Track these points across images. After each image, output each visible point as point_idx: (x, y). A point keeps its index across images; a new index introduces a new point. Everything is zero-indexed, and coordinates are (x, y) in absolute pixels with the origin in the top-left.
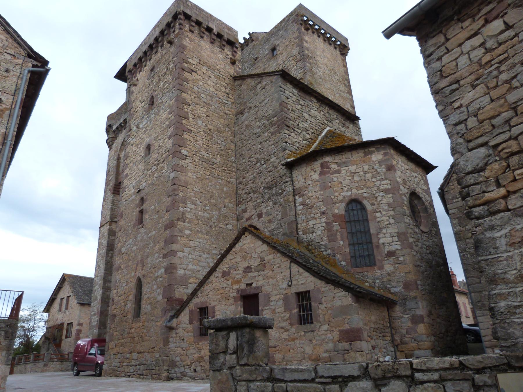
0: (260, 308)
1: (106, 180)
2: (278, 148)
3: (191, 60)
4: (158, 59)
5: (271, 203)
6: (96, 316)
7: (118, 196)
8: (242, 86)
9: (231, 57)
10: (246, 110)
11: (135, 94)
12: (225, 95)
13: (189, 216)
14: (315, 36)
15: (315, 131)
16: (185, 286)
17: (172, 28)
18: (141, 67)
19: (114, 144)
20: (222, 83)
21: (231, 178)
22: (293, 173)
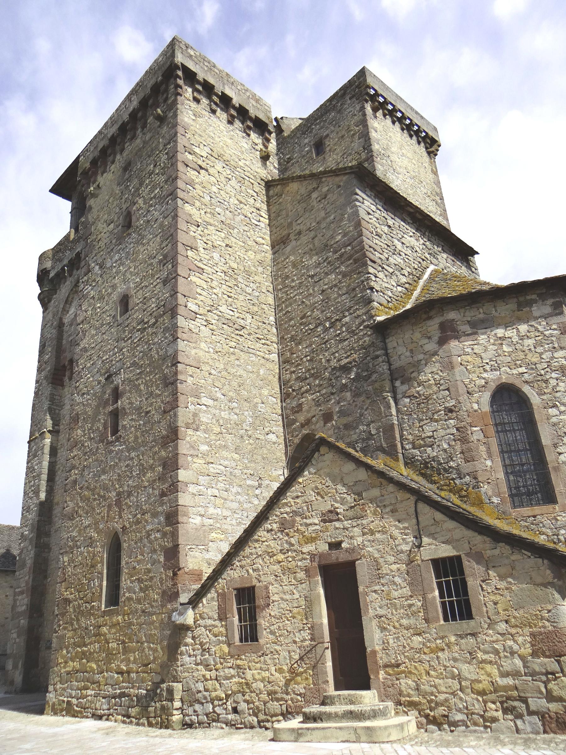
0: (361, 589)
1: (39, 362)
2: (356, 299)
3: (198, 148)
4: (137, 149)
5: (348, 394)
6: (25, 595)
7: (61, 388)
8: (283, 196)
9: (262, 147)
10: (292, 237)
11: (95, 210)
12: (255, 210)
13: (204, 418)
14: (389, 120)
15: (414, 270)
16: (203, 547)
17: (163, 94)
18: (105, 164)
19: (53, 302)
20: (248, 191)
21: (270, 352)
22: (387, 341)
